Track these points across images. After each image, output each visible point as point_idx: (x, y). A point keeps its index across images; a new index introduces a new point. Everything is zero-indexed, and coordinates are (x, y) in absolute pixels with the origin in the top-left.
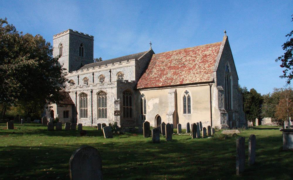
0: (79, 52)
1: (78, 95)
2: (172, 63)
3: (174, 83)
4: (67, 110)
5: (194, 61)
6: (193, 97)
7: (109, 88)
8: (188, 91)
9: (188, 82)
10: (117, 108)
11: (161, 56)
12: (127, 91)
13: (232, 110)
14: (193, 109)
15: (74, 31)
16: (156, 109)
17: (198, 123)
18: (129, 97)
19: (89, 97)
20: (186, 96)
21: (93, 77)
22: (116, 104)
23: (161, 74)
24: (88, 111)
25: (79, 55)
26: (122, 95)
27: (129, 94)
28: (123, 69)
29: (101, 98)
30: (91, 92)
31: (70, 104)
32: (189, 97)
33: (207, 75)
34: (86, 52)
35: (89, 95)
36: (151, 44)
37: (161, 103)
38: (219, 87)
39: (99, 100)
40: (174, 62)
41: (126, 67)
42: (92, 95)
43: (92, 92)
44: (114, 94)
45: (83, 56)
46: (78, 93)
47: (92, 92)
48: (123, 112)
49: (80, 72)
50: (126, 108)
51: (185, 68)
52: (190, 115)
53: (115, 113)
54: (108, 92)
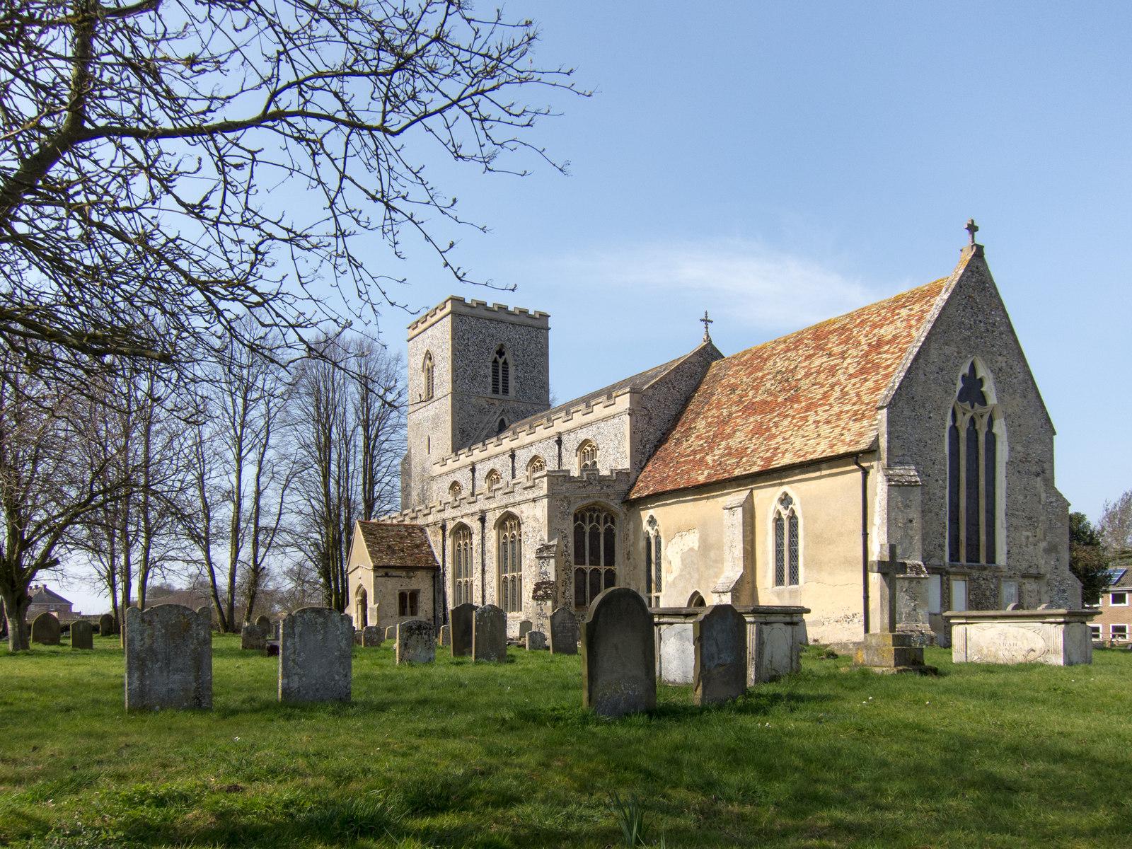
0: (490, 380)
1: (447, 533)
2: (763, 388)
3: (745, 470)
4: (415, 587)
5: (832, 371)
6: (805, 517)
7: (528, 501)
8: (791, 494)
9: (788, 460)
10: (546, 573)
11: (735, 365)
12: (594, 510)
13: (998, 569)
14: (805, 565)
15: (468, 301)
16: (690, 573)
17: (406, 595)
18: (602, 529)
19: (476, 539)
20: (785, 514)
21: (513, 467)
22: (540, 558)
23: (715, 436)
24: (474, 587)
25: (490, 389)
26: (569, 526)
27: (602, 521)
28: (594, 428)
29: (509, 539)
30: (480, 519)
31: (422, 568)
32: (793, 518)
33: (858, 425)
34: (517, 378)
35: (475, 531)
36: (706, 321)
37: (705, 546)
38: (898, 470)
39: (502, 547)
40: (768, 385)
41: (602, 420)
42: (483, 532)
43: (483, 520)
44: (541, 521)
45: (506, 391)
46: (450, 525)
47: (483, 520)
48: (576, 587)
49: (477, 454)
50: (588, 571)
51: (796, 406)
52: (796, 591)
53: (535, 591)
54: (524, 517)
